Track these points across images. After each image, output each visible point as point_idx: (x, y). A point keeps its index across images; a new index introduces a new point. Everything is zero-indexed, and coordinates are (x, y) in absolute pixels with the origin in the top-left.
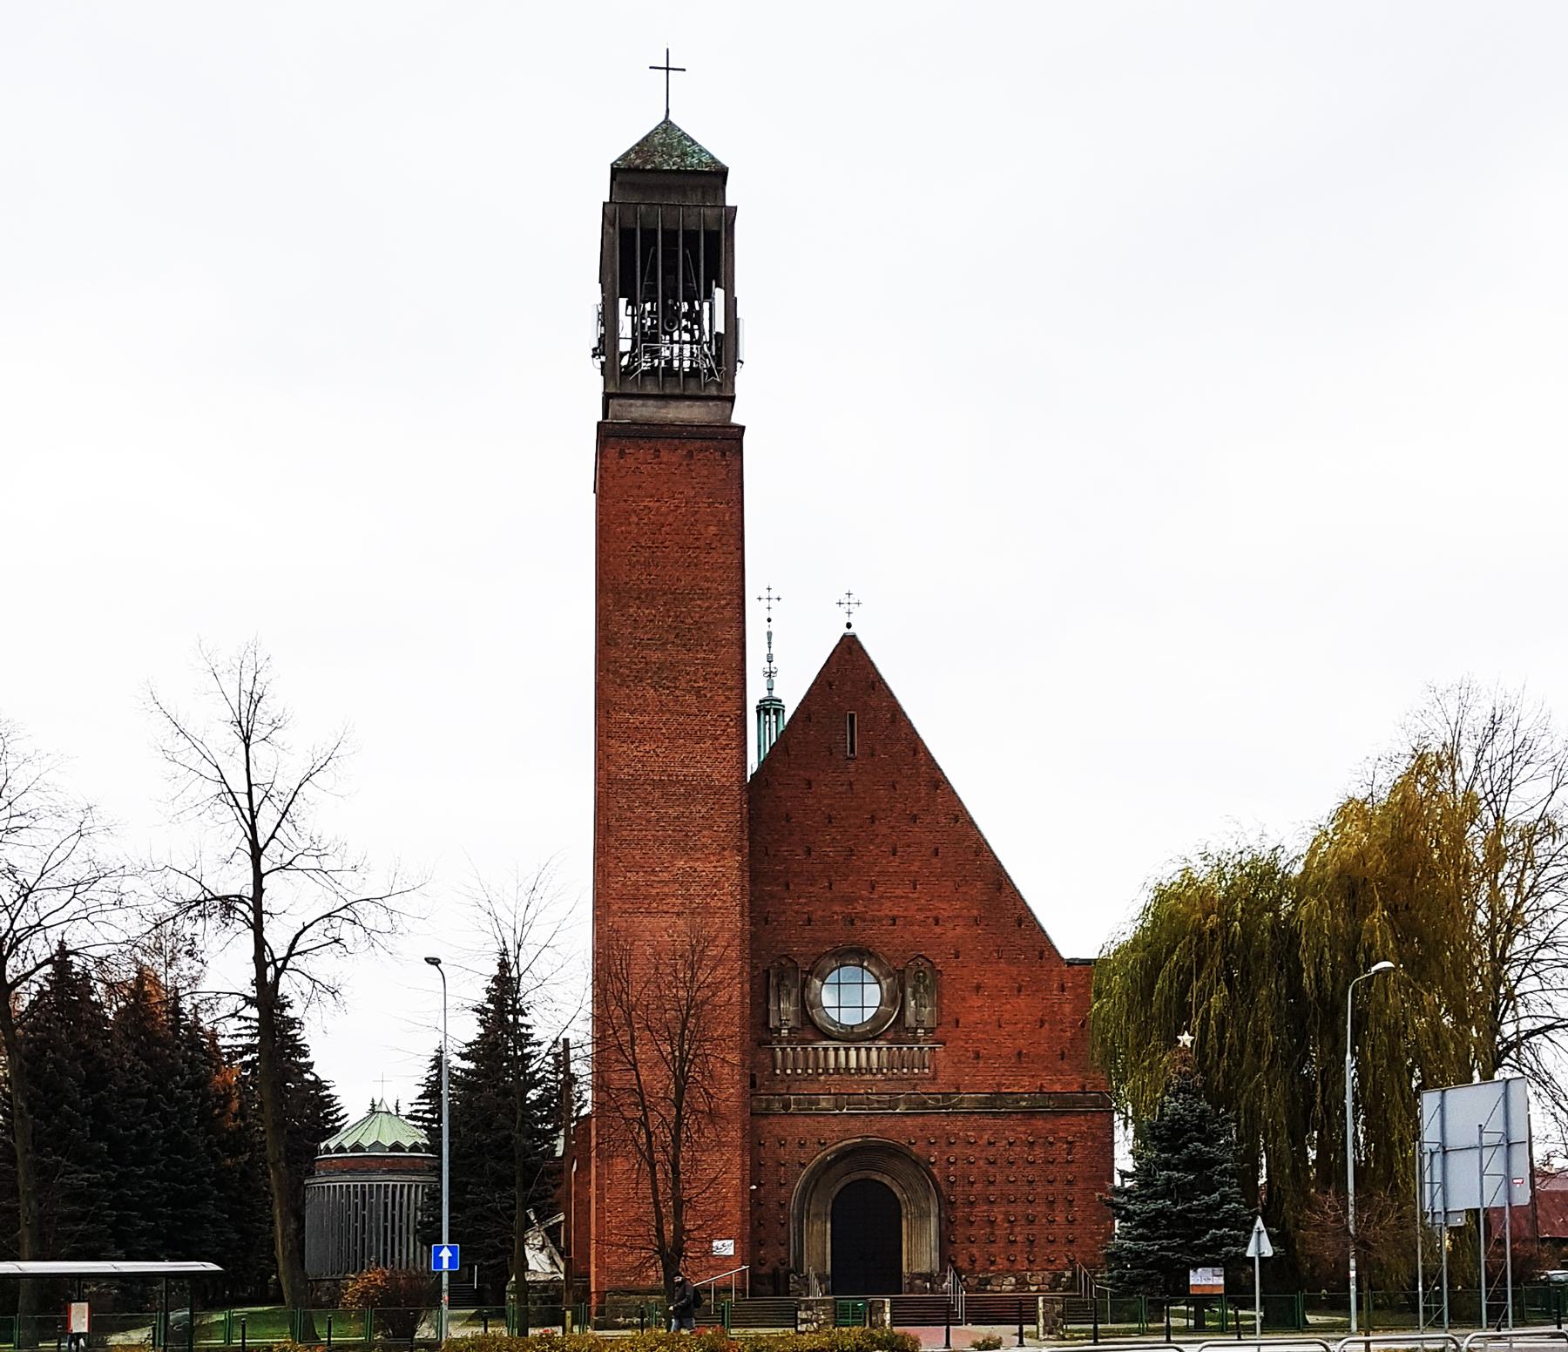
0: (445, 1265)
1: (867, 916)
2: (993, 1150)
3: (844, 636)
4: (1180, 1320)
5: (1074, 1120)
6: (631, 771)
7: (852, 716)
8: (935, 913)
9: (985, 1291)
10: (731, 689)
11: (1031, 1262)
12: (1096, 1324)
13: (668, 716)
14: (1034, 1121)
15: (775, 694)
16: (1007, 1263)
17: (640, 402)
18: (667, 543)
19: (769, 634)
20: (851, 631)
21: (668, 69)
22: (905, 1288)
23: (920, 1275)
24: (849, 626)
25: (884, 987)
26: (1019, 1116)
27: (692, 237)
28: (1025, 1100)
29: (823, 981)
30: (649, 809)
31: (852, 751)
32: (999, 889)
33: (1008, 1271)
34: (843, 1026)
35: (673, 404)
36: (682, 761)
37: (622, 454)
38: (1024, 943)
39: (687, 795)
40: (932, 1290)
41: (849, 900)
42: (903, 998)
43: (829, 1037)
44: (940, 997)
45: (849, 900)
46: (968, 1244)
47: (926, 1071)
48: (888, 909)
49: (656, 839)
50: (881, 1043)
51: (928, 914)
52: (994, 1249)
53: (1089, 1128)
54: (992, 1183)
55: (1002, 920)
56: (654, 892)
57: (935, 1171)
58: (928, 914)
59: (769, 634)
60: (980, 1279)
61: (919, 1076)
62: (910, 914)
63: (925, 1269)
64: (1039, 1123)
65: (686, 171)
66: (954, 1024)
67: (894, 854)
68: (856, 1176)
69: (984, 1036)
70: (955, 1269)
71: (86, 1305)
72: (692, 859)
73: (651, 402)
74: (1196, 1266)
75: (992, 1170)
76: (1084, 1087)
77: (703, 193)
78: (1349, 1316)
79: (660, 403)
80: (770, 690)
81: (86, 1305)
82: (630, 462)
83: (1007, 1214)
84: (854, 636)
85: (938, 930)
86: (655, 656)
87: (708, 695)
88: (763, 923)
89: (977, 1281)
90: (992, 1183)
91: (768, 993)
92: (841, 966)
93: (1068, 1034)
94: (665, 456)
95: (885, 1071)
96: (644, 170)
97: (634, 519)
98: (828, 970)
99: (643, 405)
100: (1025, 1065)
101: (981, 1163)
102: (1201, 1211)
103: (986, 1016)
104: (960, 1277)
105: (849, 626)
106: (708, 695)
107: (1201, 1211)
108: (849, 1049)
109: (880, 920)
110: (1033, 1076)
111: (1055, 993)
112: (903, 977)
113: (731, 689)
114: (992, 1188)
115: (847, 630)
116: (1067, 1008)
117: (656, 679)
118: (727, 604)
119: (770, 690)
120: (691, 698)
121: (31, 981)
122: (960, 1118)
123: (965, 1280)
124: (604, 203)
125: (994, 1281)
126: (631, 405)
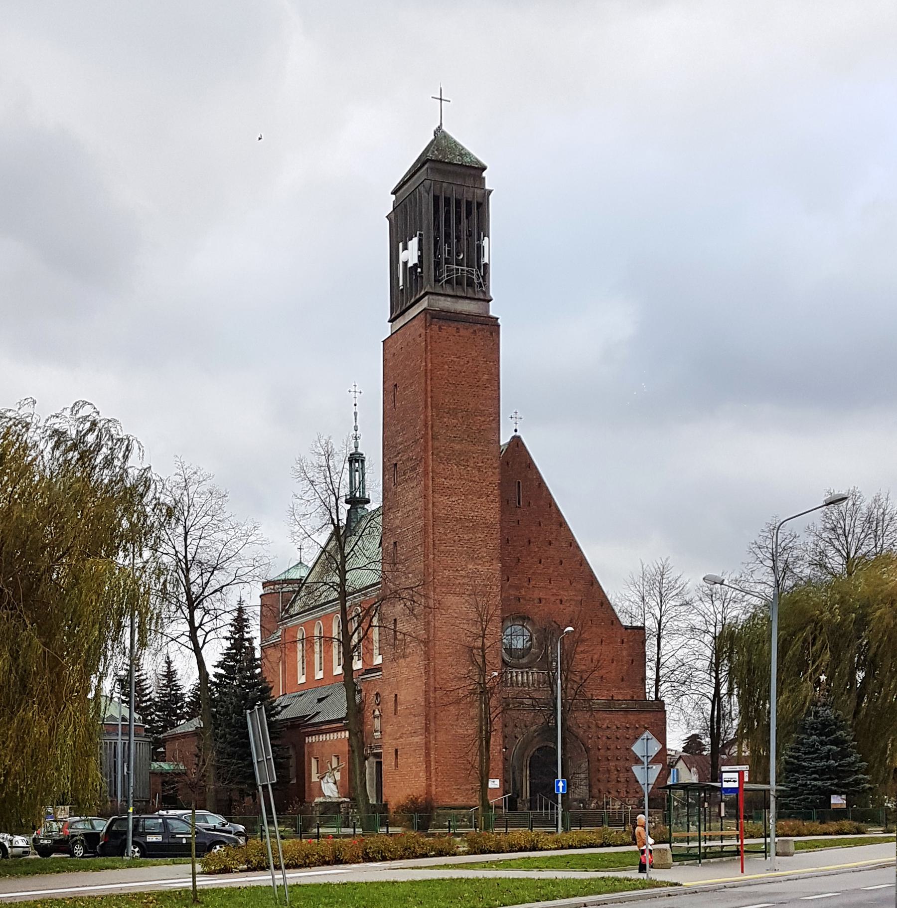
0: (561, 790)
2: (609, 731)
3: (514, 437)
5: (648, 716)
6: (446, 512)
7: (519, 483)
10: (495, 468)
11: (627, 792)
13: (464, 482)
14: (629, 716)
15: (359, 450)
16: (616, 794)
17: (443, 298)
18: (463, 383)
19: (356, 413)
20: (518, 434)
21: (441, 99)
24: (516, 431)
26: (622, 713)
27: (469, 204)
30: (455, 534)
31: (519, 503)
32: (592, 585)
35: (460, 301)
36: (471, 508)
37: (440, 329)
38: (603, 616)
39: (474, 527)
41: (518, 588)
45: (518, 588)
48: (537, 594)
49: (458, 551)
51: (557, 597)
52: (609, 785)
56: (457, 582)
59: (356, 413)
62: (548, 597)
64: (631, 717)
65: (466, 166)
67: (540, 563)
72: (476, 564)
73: (449, 299)
74: (835, 793)
76: (633, 697)
77: (474, 179)
79: (454, 300)
80: (356, 448)
82: (444, 333)
83: (616, 766)
84: (519, 437)
85: (562, 607)
86: (457, 447)
87: (484, 471)
94: (463, 332)
96: (444, 162)
97: (446, 367)
99: (445, 300)
101: (604, 738)
102: (846, 766)
105: (516, 431)
106: (484, 471)
107: (846, 766)
109: (533, 600)
113: (495, 468)
116: (625, 653)
117: (457, 460)
118: (493, 420)
119: (356, 448)
120: (475, 472)
121: (199, 626)
126: (438, 300)
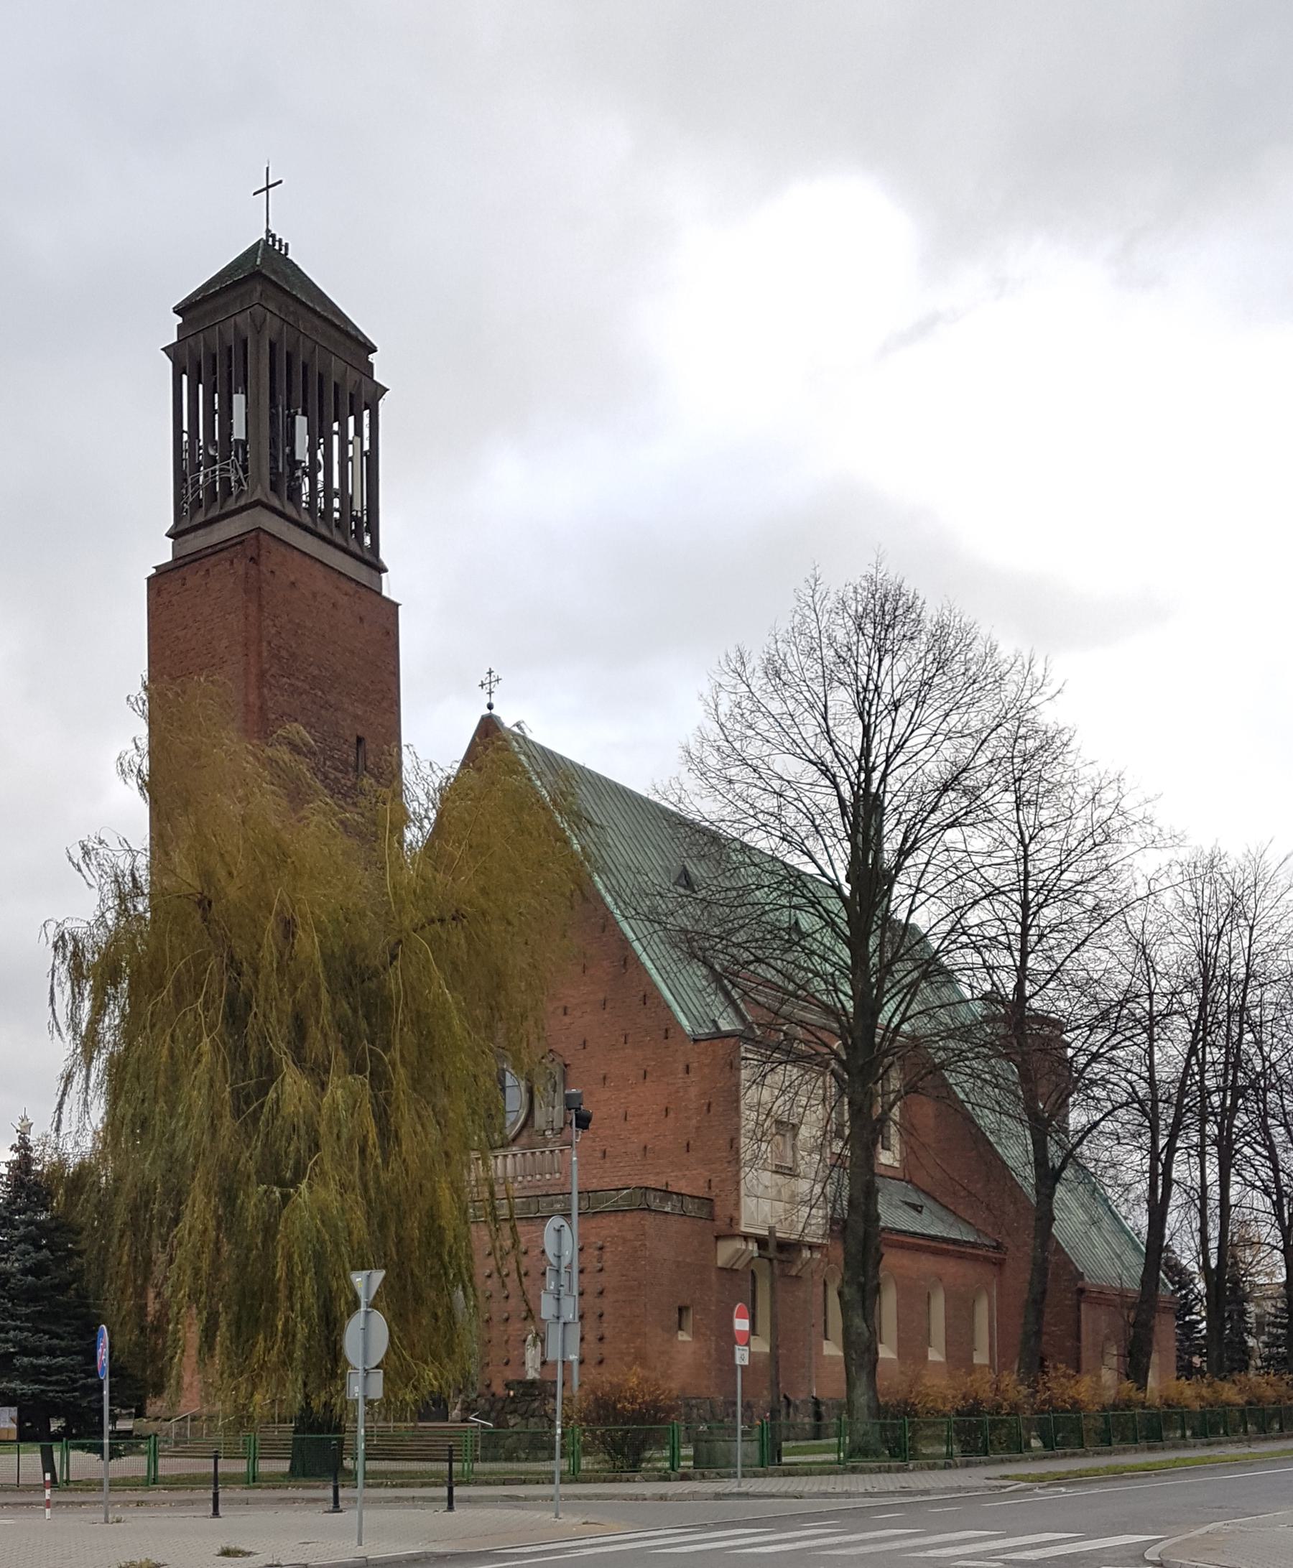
4: (937, 1447)
12: (451, 1461)
24: (490, 707)
28: (558, 1202)
35: (216, 526)
47: (557, 1175)
50: (515, 1149)
53: (620, 1231)
61: (550, 1182)
71: (16, 1408)
79: (208, 529)
81: (16, 1408)
85: (567, 1020)
93: (694, 1121)
95: (520, 1178)
100: (650, 1162)
105: (490, 707)
110: (658, 1174)
111: (680, 1076)
115: (488, 711)
116: (693, 1092)
124: (374, 350)
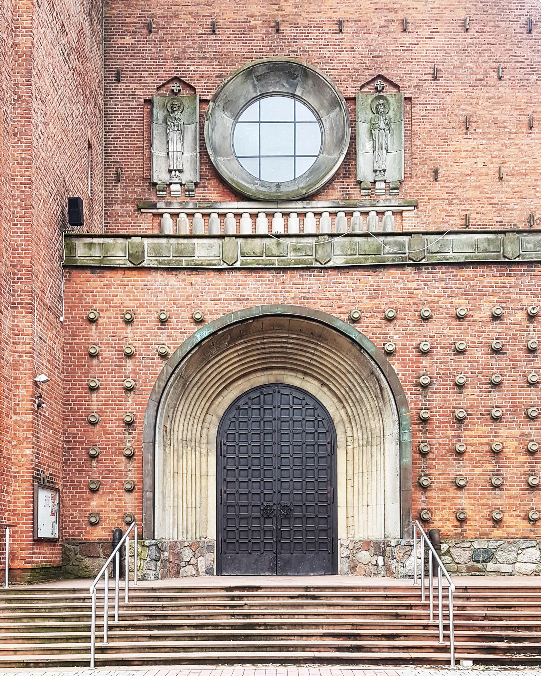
1: (300, 21)
8: (401, 15)
9: (482, 572)
16: (523, 526)
22: (343, 564)
23: (367, 544)
25: (327, 125)
29: (236, 117)
33: (526, 538)
34: (263, 184)
40: (389, 572)
42: (354, 139)
43: (241, 196)
44: (410, 137)
46: (452, 492)
51: (392, 16)
54: (496, 385)
55: (503, 24)
57: (396, 367)
58: (392, 16)
60: (475, 551)
63: (377, 534)
66: (430, 175)
68: (261, 379)
69: (477, 194)
70: (430, 535)
75: (496, 362)
78: (429, 592)
85: (406, 39)
88: (145, 31)
89: (469, 554)
90: (496, 385)
91: (151, 134)
92: (263, 96)
98: (242, 102)
103: (480, 165)
104: (438, 549)
108: (273, 215)
112: (354, 111)
114: (495, 395)
122: (440, 276)
123: (448, 552)
125: (500, 555)
